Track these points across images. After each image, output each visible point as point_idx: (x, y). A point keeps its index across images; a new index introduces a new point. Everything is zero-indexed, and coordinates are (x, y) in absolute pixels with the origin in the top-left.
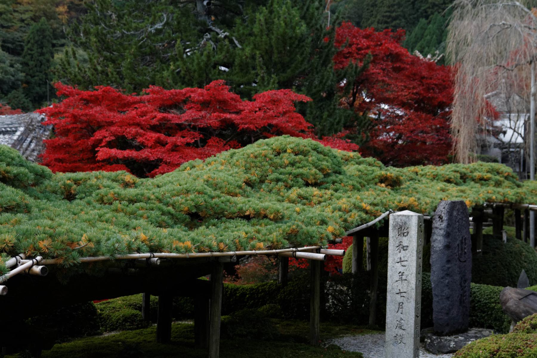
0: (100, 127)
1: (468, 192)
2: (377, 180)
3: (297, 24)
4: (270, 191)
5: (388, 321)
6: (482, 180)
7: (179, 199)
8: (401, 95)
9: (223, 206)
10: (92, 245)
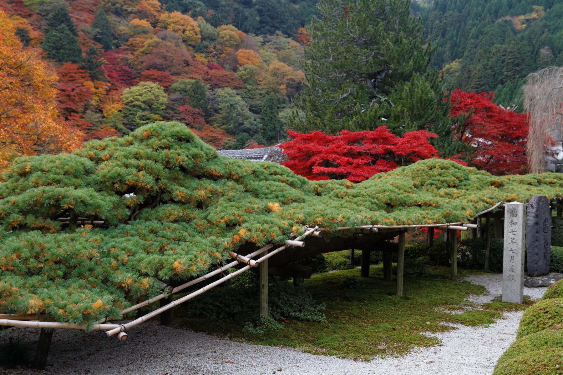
0: (314, 154)
1: (544, 190)
2: (489, 184)
3: (428, 91)
4: (428, 190)
5: (504, 266)
6: (551, 183)
7: (380, 195)
8: (493, 132)
9: (405, 199)
10: (344, 220)
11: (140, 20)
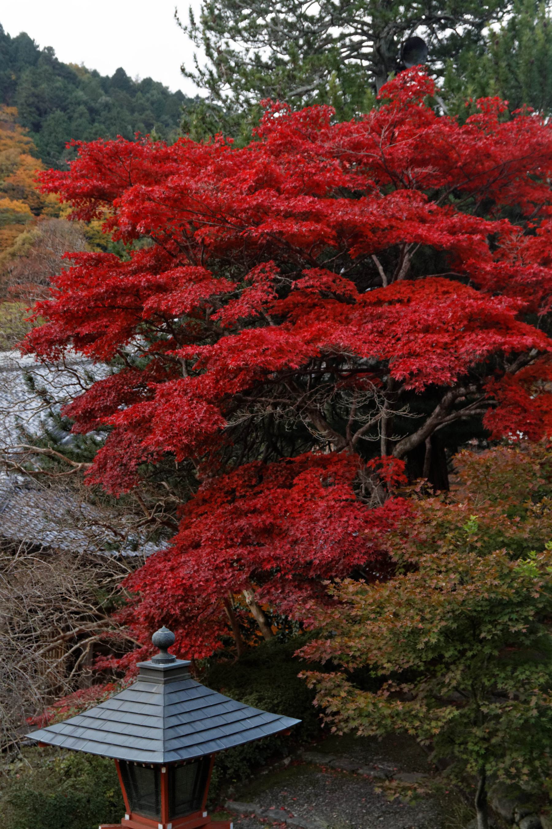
11: (12, 201)
